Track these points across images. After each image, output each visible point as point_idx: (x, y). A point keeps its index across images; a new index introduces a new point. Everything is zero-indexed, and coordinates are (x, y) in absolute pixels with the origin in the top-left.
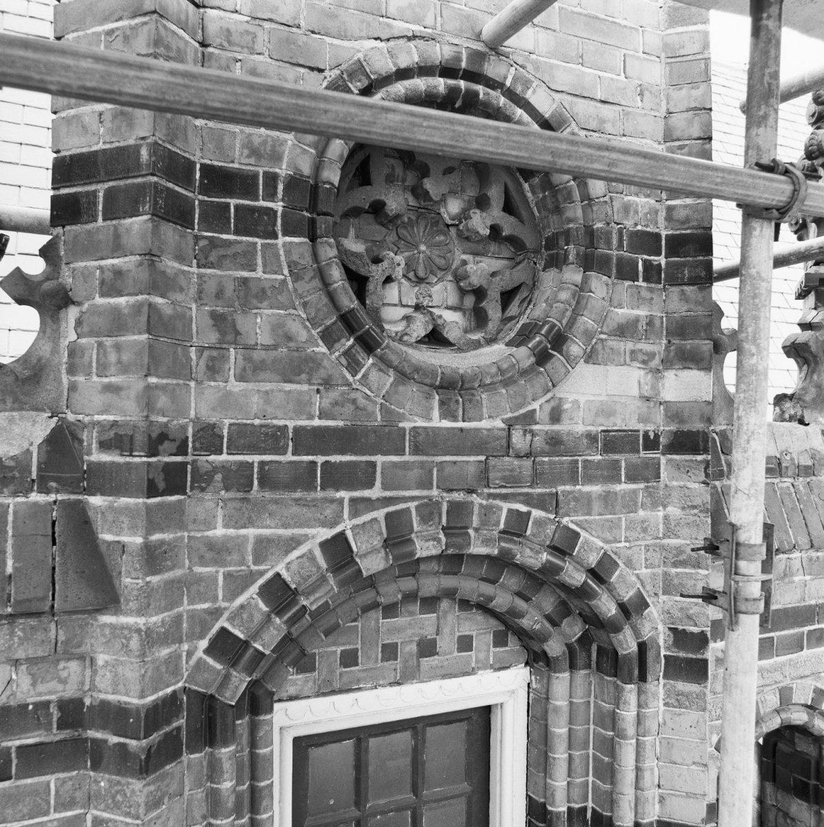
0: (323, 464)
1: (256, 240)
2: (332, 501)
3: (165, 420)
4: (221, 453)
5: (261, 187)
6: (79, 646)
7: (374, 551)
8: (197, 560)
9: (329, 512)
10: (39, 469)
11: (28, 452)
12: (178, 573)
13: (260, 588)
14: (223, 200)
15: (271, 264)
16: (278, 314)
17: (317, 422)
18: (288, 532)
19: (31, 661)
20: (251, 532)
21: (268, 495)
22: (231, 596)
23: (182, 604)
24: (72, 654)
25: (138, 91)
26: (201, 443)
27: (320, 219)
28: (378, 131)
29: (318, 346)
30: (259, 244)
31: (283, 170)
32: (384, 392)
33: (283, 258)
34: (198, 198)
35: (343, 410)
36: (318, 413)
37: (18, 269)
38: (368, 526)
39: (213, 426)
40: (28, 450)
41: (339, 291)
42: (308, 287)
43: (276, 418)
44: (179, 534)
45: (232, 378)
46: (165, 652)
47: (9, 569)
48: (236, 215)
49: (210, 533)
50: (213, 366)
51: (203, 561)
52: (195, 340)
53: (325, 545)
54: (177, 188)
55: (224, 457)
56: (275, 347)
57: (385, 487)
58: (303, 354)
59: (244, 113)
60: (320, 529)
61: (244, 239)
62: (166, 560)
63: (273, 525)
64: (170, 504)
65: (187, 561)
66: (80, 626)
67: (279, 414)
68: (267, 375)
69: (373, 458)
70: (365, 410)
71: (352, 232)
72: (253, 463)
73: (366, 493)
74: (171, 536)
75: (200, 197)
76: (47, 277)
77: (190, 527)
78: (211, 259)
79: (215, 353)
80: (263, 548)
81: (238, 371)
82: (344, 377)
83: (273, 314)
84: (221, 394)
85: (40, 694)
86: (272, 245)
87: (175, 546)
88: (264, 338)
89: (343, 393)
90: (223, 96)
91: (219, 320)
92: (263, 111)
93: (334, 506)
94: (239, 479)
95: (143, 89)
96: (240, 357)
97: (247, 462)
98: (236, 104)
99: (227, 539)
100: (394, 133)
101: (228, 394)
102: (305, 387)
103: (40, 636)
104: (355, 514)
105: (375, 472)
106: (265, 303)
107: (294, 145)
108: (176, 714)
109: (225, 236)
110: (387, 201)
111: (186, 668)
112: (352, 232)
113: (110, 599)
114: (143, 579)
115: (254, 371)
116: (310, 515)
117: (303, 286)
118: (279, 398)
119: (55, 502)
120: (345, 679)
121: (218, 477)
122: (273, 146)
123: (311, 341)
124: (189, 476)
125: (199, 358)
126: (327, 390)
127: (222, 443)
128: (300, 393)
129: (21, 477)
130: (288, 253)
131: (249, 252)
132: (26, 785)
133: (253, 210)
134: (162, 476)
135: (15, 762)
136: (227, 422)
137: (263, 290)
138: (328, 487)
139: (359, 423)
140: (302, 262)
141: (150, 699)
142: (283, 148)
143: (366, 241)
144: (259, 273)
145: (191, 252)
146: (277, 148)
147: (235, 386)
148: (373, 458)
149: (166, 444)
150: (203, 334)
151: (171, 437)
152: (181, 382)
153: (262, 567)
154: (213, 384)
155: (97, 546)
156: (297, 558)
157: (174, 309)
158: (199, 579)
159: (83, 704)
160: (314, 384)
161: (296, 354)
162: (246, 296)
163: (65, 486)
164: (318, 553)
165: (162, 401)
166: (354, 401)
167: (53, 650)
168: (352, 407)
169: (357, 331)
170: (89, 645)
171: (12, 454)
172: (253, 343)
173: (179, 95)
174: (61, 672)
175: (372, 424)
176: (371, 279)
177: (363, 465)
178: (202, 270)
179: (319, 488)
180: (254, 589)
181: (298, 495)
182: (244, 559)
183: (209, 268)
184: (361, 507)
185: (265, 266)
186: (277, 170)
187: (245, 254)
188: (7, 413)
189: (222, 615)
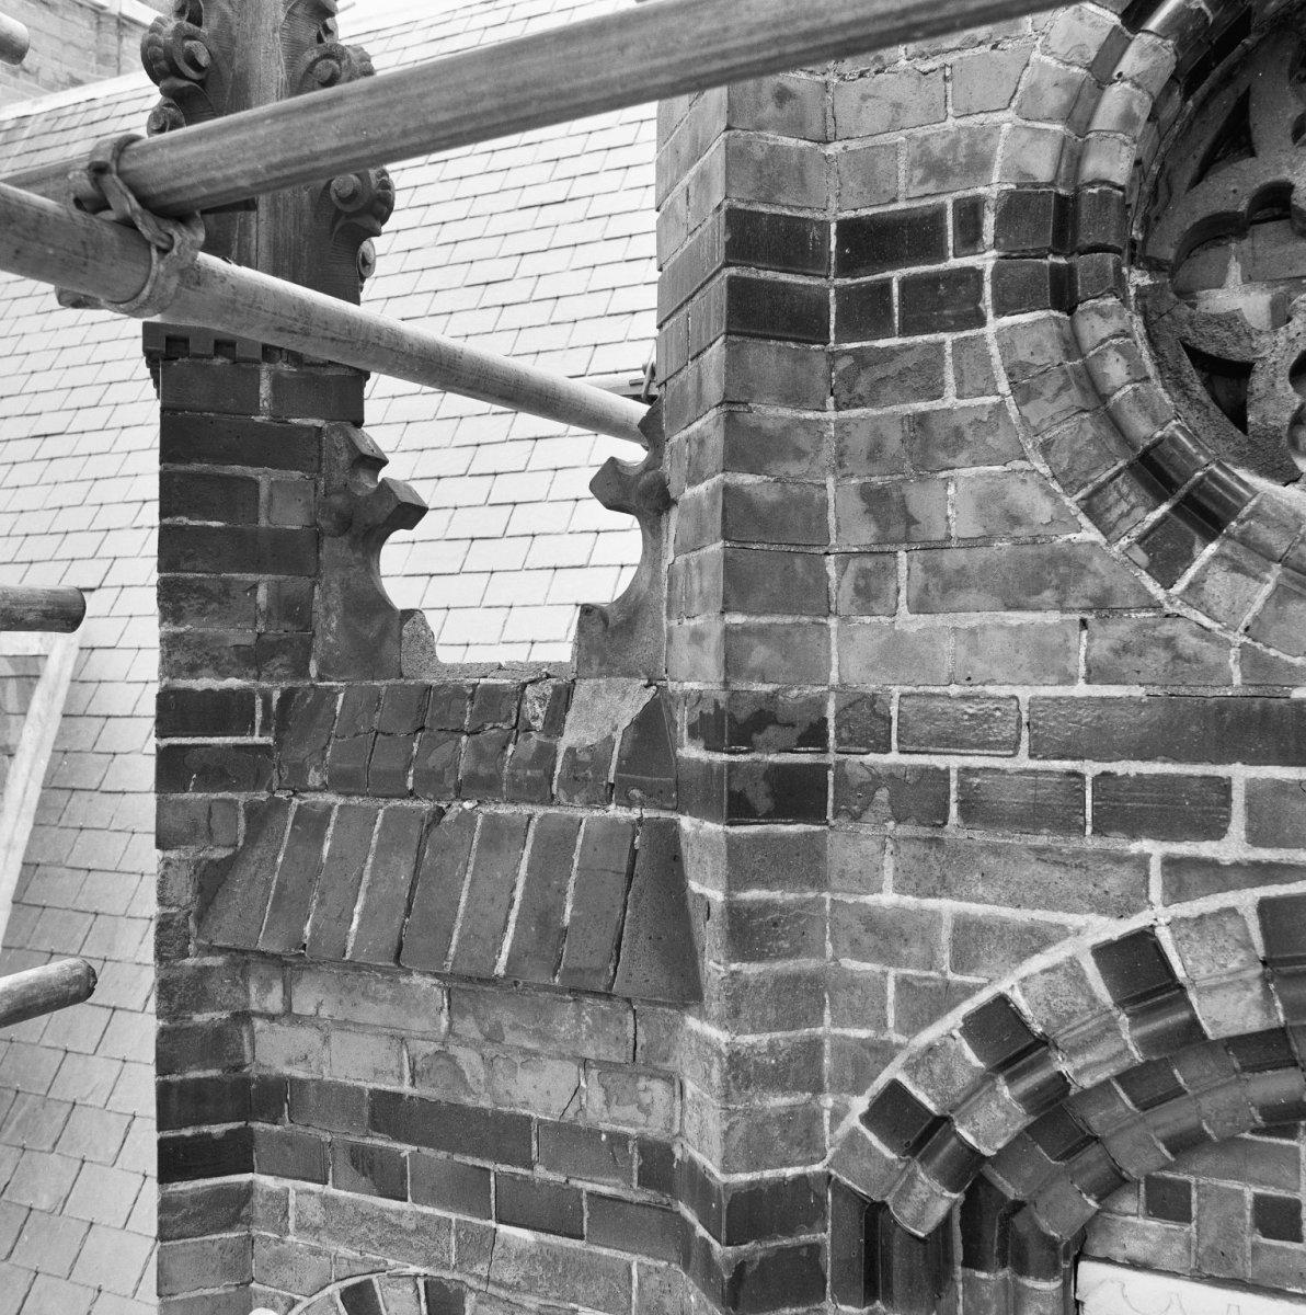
0: (1096, 779)
1: (942, 336)
2: (1120, 859)
3: (768, 688)
4: (888, 750)
5: (950, 232)
6: (666, 1060)
7: (1236, 982)
8: (846, 945)
9: (1115, 881)
10: (619, 769)
11: (609, 740)
12: (808, 964)
13: (965, 1020)
14: (878, 276)
15: (975, 378)
16: (990, 474)
17: (1081, 689)
18: (1022, 916)
19: (606, 1067)
20: (947, 907)
21: (979, 836)
22: (913, 1025)
23: (820, 1022)
24: (655, 1068)
25: (334, 143)
26: (850, 731)
27: (1081, 261)
28: (741, 42)
29: (1079, 529)
30: (949, 343)
31: (993, 187)
32: (1247, 618)
33: (996, 361)
34: (832, 285)
35: (1140, 663)
36: (1082, 670)
37: (612, 460)
38: (1211, 925)
39: (873, 699)
40: (610, 737)
41: (1126, 406)
42: (1051, 409)
43: (992, 682)
44: (811, 895)
45: (903, 609)
46: (778, 1102)
47: (567, 920)
48: (902, 297)
49: (870, 899)
50: (867, 586)
51: (858, 953)
52: (833, 542)
53: (1103, 952)
54: (783, 277)
55: (894, 757)
56: (986, 540)
57: (1255, 838)
58: (1045, 550)
59: (488, 113)
60: (1092, 917)
61: (919, 339)
62: (778, 938)
63: (990, 898)
64: (783, 838)
65: (829, 946)
66: (667, 1027)
67: (998, 673)
68: (971, 597)
69: (1221, 771)
70: (1198, 661)
71: (1235, 271)
72: (947, 771)
73: (1206, 849)
74: (791, 896)
75: (838, 282)
76: (651, 465)
77: (835, 883)
78: (859, 390)
79: (869, 563)
80: (971, 940)
81: (914, 593)
82: (1142, 590)
83: (979, 476)
84: (884, 638)
85: (615, 1121)
86: (973, 339)
87: (799, 916)
88: (964, 525)
89: (1141, 627)
90: (446, 97)
91: (876, 501)
92: (514, 98)
93: (1126, 871)
94: (921, 800)
95: (340, 136)
96: (917, 566)
97: (937, 769)
98: (469, 103)
99: (904, 913)
100: (775, 33)
101: (898, 639)
102: (1054, 617)
103: (612, 1029)
104: (1176, 893)
105: (1227, 801)
106: (963, 456)
107: (1015, 128)
108: (813, 1217)
109: (882, 343)
110: (1295, 180)
111: (831, 1138)
112: (1235, 271)
113: (689, 993)
114: (726, 965)
115: (945, 590)
116: (1070, 885)
117: (1039, 411)
118: (997, 642)
119: (640, 820)
120: (1266, 1261)
121: (882, 795)
122: (971, 146)
123: (1061, 520)
124: (831, 790)
125: (842, 572)
126: (1103, 620)
127: (889, 732)
128: (1044, 629)
129: (595, 780)
130: (1007, 348)
131: (929, 362)
132: (600, 1256)
133: (932, 281)
134: (763, 787)
135: (586, 1215)
136: (896, 691)
137: (958, 432)
138: (1110, 829)
139: (1183, 690)
140: (1038, 360)
141: (743, 1177)
142: (991, 142)
143: (1273, 282)
144: (950, 400)
145: (821, 384)
146: (980, 147)
147: (909, 622)
148: (1221, 771)
149: (771, 731)
150: (847, 527)
151: (781, 717)
152: (805, 619)
153: (970, 979)
154: (867, 619)
155: (685, 899)
156: (1044, 971)
157: (784, 490)
158: (852, 983)
159: (673, 1155)
160: (1071, 610)
161: (1030, 550)
162: (925, 447)
163: (654, 797)
164: (1090, 967)
165: (760, 654)
166: (1169, 643)
167: (631, 1057)
168: (1164, 656)
169: (1178, 487)
170: (678, 1061)
171: (588, 743)
172: (940, 535)
173: (385, 125)
174: (642, 1095)
175: (1220, 692)
176: (1259, 365)
177: (1197, 784)
178: (844, 414)
179: (1089, 829)
180: (953, 1020)
181: (1042, 840)
182: (933, 955)
183: (857, 406)
184: (1192, 878)
185: (960, 383)
186: (981, 190)
187: (920, 368)
188: (592, 682)
189: (892, 1057)
